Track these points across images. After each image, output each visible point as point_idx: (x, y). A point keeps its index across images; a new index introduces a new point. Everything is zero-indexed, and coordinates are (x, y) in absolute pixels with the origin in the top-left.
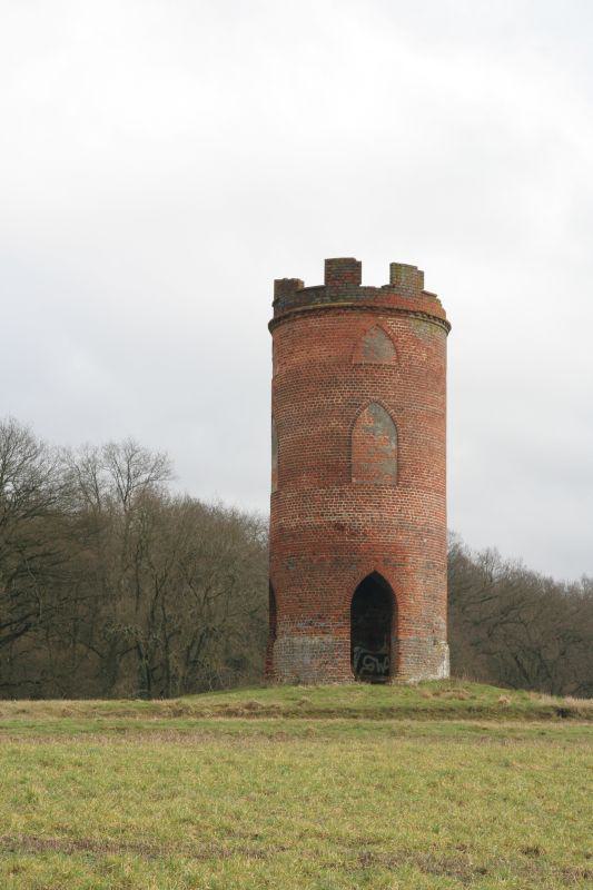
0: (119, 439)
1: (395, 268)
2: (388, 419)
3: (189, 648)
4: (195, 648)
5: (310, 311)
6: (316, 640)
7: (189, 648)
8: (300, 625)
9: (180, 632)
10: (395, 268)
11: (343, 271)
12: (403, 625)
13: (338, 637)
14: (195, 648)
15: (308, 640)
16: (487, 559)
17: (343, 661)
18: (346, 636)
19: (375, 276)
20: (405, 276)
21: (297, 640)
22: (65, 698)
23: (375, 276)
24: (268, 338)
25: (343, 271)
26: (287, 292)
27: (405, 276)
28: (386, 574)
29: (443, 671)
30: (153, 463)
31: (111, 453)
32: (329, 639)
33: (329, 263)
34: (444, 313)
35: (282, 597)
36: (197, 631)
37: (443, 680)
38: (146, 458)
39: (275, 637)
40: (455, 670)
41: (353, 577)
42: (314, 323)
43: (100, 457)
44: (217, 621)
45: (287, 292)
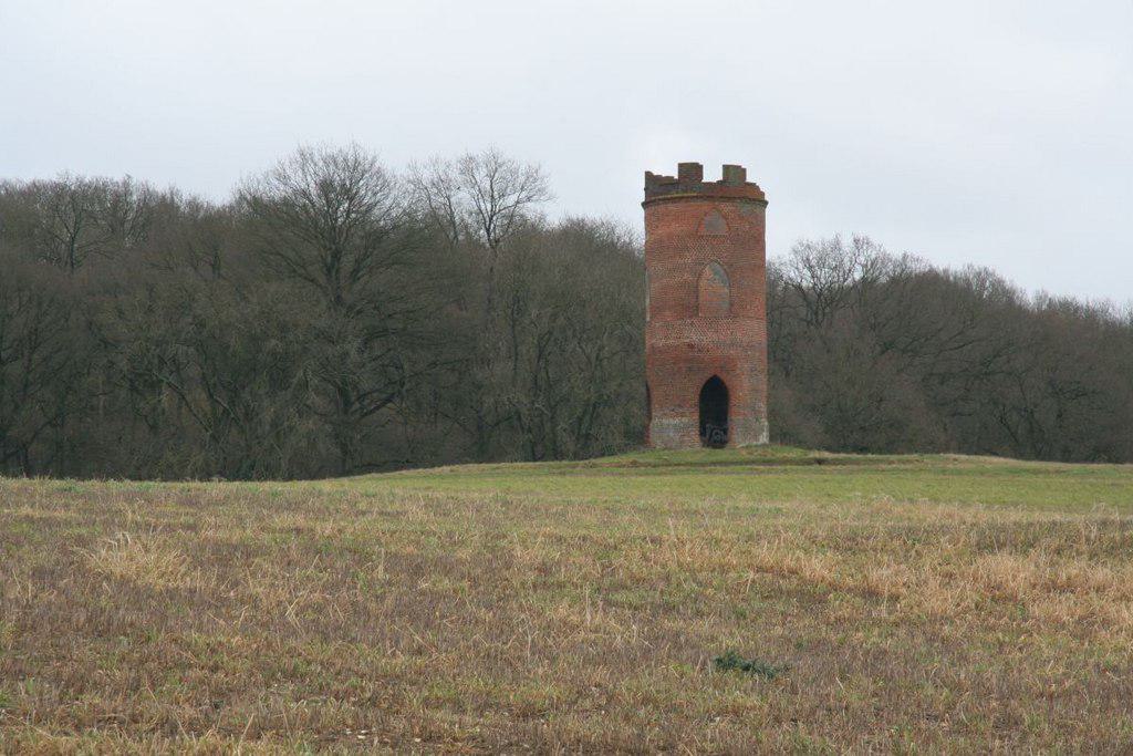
0: (479, 150)
1: (726, 168)
2: (722, 272)
3: (580, 419)
4: (587, 417)
5: (669, 199)
6: (677, 421)
7: (580, 419)
8: (667, 411)
9: (569, 401)
10: (726, 168)
11: (691, 171)
12: (734, 409)
13: (691, 419)
14: (587, 417)
15: (672, 421)
16: (945, 271)
17: (695, 433)
18: (696, 417)
19: (712, 175)
20: (734, 173)
21: (665, 421)
22: (1016, 457)
23: (712, 175)
24: (641, 212)
25: (691, 171)
26: (652, 180)
27: (734, 173)
28: (723, 376)
29: (764, 438)
30: (522, 179)
31: (468, 166)
32: (685, 420)
33: (681, 165)
34: (763, 194)
35: (655, 394)
36: (589, 399)
37: (764, 445)
38: (514, 172)
39: (650, 419)
40: (772, 438)
41: (700, 380)
42: (671, 207)
43: (455, 174)
44: (613, 386)
45: (652, 180)
